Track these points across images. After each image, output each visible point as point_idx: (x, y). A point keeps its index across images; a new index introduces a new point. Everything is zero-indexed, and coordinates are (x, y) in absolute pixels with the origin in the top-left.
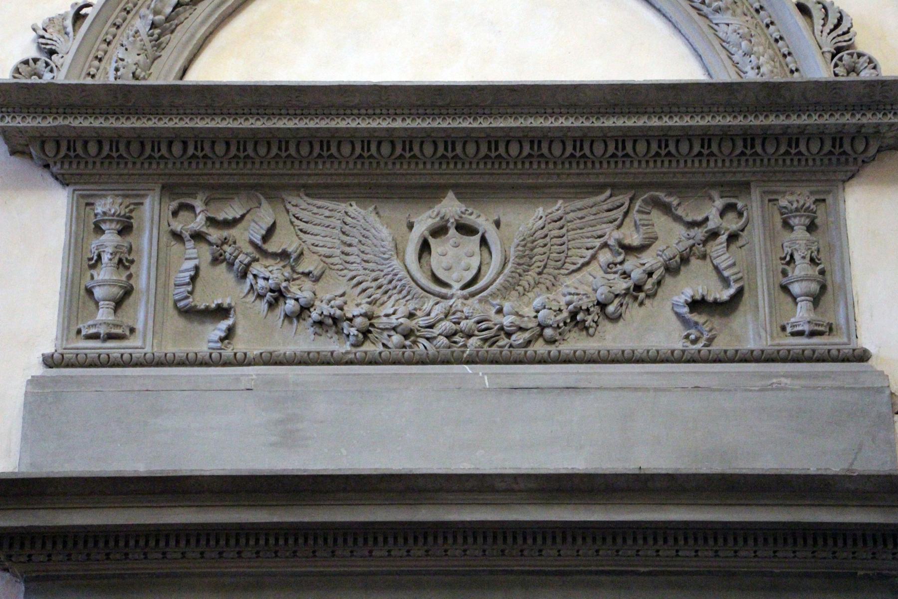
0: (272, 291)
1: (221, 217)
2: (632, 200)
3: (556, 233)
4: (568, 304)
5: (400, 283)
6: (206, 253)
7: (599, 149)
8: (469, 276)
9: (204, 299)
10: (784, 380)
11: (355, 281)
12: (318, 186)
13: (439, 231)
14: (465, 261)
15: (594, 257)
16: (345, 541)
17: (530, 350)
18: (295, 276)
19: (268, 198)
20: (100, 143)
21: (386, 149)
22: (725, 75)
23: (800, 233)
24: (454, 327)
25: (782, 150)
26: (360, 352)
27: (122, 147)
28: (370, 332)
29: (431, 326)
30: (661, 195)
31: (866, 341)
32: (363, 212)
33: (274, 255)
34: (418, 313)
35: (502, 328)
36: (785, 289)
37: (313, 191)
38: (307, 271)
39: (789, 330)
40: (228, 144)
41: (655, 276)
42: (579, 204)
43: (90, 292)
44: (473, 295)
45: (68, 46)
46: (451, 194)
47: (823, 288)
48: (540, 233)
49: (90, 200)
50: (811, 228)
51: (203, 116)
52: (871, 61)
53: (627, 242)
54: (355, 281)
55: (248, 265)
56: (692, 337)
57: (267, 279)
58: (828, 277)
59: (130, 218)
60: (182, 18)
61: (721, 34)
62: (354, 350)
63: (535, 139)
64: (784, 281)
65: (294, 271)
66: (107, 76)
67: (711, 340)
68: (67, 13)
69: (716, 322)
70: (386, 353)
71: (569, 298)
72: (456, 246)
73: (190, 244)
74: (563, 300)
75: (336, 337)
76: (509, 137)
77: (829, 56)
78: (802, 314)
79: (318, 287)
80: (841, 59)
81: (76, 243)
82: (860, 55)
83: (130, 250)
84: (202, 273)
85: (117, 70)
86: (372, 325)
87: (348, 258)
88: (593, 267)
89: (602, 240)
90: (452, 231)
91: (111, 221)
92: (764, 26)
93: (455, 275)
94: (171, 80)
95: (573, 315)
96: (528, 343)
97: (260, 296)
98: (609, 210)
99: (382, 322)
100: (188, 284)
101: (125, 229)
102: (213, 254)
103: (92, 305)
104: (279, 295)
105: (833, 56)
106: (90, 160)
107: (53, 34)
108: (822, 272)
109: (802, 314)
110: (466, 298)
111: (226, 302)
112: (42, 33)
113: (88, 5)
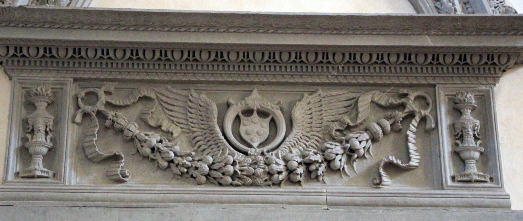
27: (330, 56)
106: (32, 61)
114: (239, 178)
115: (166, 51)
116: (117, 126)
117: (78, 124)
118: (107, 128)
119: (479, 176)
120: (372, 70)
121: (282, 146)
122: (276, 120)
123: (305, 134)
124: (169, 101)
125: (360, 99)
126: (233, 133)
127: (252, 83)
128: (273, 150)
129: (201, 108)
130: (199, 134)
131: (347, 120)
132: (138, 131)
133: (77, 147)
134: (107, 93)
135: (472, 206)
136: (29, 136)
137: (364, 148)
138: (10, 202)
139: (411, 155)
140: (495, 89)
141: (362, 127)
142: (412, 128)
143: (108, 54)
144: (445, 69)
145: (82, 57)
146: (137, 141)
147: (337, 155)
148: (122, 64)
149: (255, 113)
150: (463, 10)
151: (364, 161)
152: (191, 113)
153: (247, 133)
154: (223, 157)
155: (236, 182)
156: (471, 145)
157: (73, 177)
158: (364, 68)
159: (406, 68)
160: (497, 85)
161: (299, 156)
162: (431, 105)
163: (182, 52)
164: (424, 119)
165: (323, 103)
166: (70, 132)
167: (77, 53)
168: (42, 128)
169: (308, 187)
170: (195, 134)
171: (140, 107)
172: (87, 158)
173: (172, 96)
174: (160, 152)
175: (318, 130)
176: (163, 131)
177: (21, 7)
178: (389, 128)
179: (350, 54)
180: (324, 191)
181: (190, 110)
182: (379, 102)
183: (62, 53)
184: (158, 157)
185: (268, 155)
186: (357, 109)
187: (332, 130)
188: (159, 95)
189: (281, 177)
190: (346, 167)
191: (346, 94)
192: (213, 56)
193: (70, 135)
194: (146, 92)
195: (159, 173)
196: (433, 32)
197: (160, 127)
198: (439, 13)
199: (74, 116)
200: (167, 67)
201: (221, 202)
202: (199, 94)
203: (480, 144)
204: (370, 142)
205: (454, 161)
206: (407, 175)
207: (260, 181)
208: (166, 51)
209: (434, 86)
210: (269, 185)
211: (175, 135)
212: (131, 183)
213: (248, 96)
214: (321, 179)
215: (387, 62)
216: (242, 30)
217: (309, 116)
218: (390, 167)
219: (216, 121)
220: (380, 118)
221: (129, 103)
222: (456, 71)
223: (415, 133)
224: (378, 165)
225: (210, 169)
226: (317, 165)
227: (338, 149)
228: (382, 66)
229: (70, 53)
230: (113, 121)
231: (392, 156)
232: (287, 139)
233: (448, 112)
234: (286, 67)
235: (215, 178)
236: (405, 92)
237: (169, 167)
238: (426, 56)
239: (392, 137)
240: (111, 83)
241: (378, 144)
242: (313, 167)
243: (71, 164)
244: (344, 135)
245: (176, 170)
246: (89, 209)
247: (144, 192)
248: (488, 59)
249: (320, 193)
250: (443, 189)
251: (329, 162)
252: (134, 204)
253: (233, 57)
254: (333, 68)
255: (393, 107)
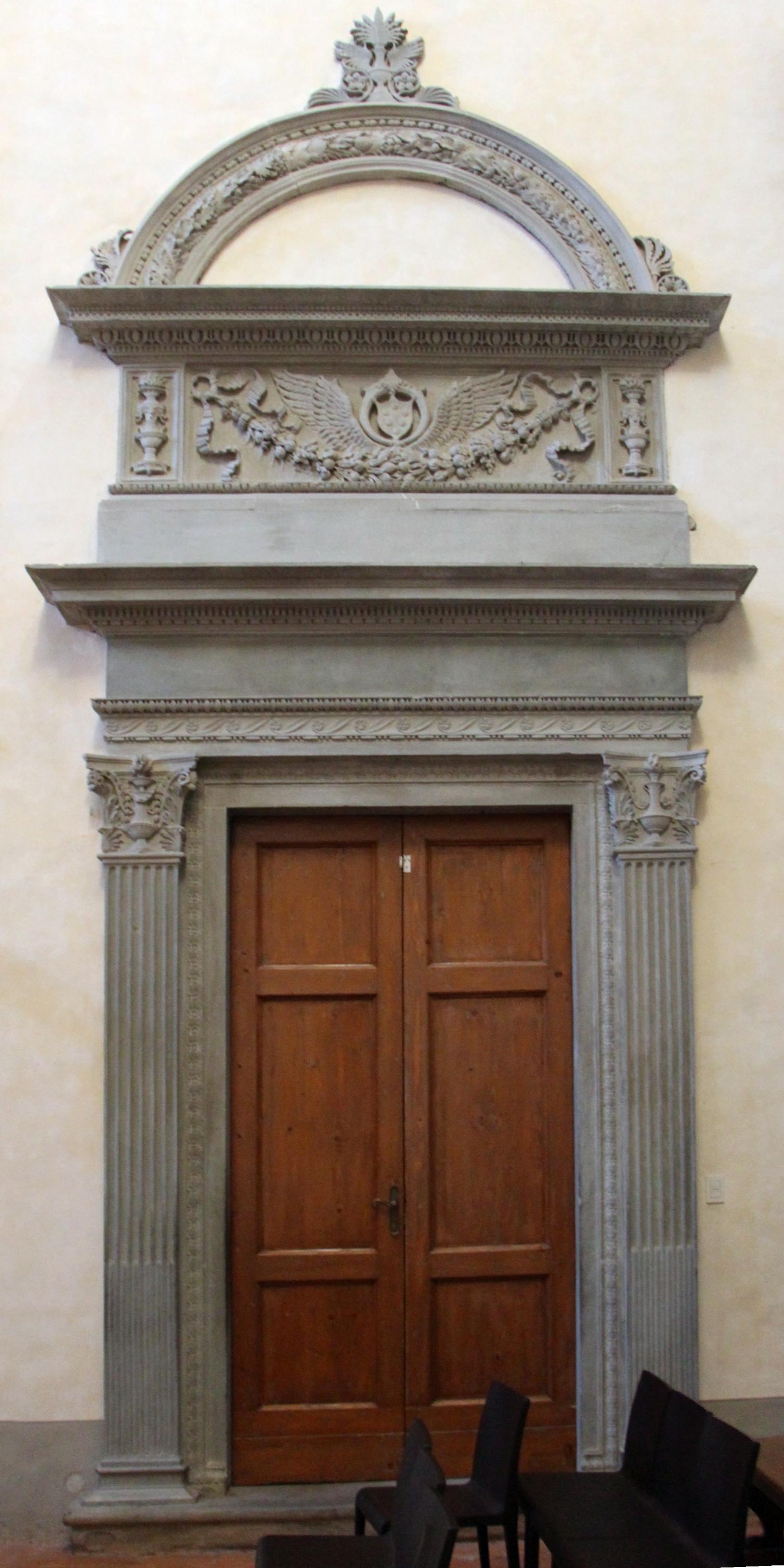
0: (265, 440)
1: (228, 386)
2: (520, 378)
3: (466, 400)
4: (474, 451)
5: (355, 435)
6: (217, 413)
7: (496, 338)
8: (404, 430)
9: (217, 446)
10: (620, 506)
11: (324, 434)
12: (296, 364)
13: (383, 398)
14: (403, 419)
15: (492, 418)
16: (321, 613)
17: (448, 484)
18: (282, 430)
19: (261, 373)
20: (141, 333)
21: (345, 337)
22: (584, 287)
23: (634, 404)
24: (395, 466)
25: (623, 344)
26: (328, 484)
28: (335, 470)
29: (378, 466)
30: (540, 375)
31: (674, 480)
32: (329, 383)
33: (266, 415)
34: (369, 456)
35: (428, 468)
36: (622, 443)
37: (294, 368)
38: (289, 426)
39: (624, 472)
40: (231, 333)
41: (535, 433)
42: (482, 379)
43: (138, 441)
44: (407, 444)
45: (117, 263)
46: (391, 372)
47: (648, 443)
48: (455, 400)
49: (136, 375)
50: (641, 401)
51: (213, 311)
52: (683, 283)
53: (516, 407)
54: (324, 434)
55: (248, 422)
56: (559, 476)
57: (261, 431)
58: (651, 436)
59: (164, 388)
60: (196, 240)
61: (582, 259)
62: (323, 482)
63: (451, 331)
64: (622, 438)
65: (280, 425)
66: (145, 282)
67: (571, 479)
68: (115, 239)
69: (576, 465)
70: (346, 484)
71: (475, 447)
72: (396, 408)
73: (207, 406)
74: (471, 449)
75: (311, 473)
76: (432, 329)
77: (655, 278)
78: (633, 461)
79: (298, 438)
80: (663, 281)
81: (127, 407)
82: (676, 279)
83: (165, 411)
84: (216, 427)
85: (151, 279)
86: (337, 465)
87: (318, 417)
88: (492, 426)
89: (498, 406)
90: (393, 398)
91: (151, 390)
92: (611, 254)
93: (395, 430)
94: (191, 284)
95: (478, 459)
96: (446, 478)
97: (257, 444)
98: (504, 385)
99: (343, 463)
100: (205, 435)
101: (161, 396)
102: (223, 414)
103: (140, 450)
104: (270, 443)
105: (659, 278)
107: (105, 254)
108: (648, 432)
109: (633, 461)
110: (402, 446)
111: (233, 447)
112: (98, 253)
113: (129, 232)
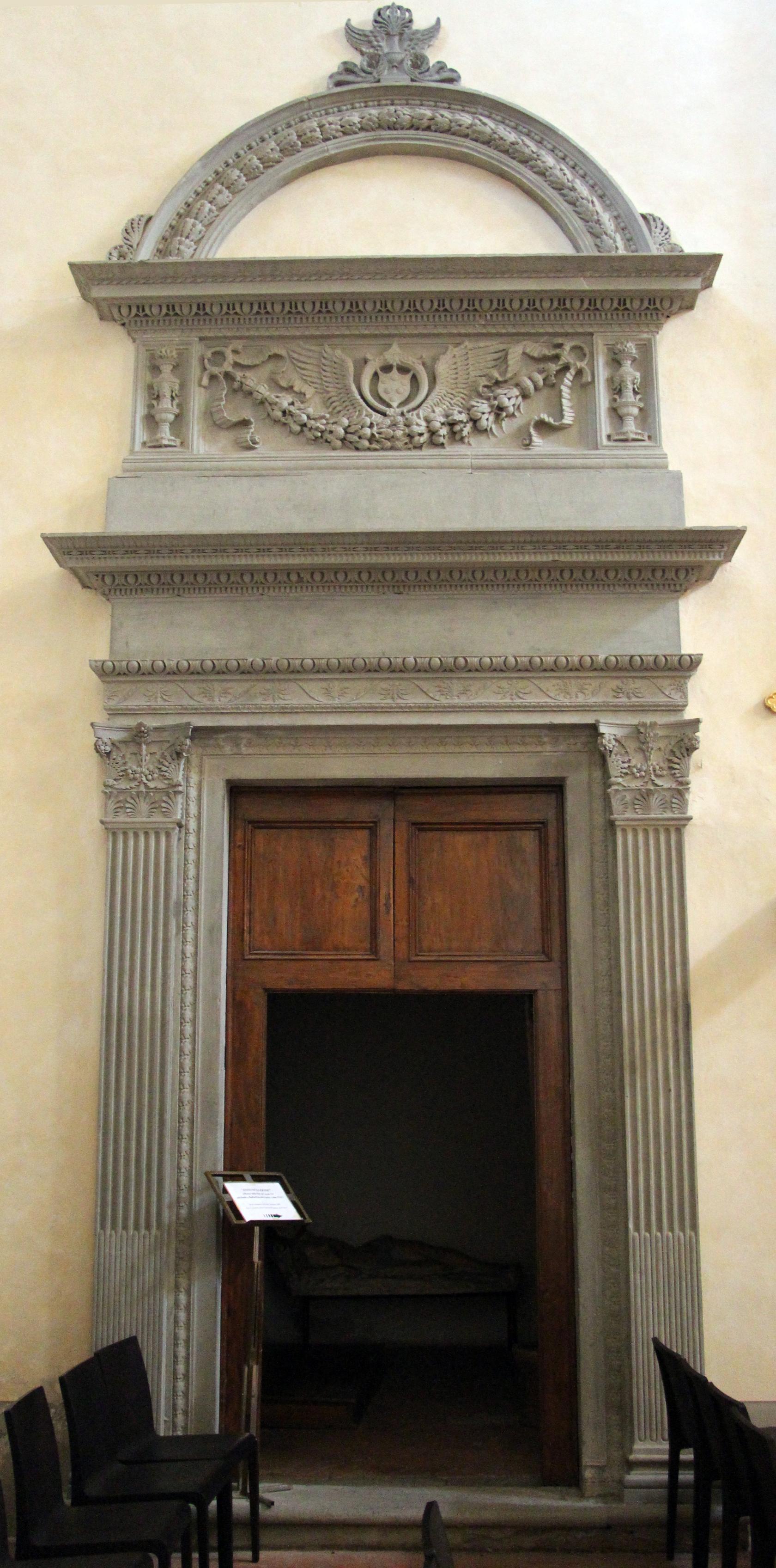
114: (377, 442)
115: (296, 304)
116: (245, 388)
117: (205, 387)
118: (235, 391)
119: (636, 434)
120: (523, 318)
121: (424, 405)
122: (418, 377)
123: (450, 391)
124: (302, 359)
125: (510, 351)
126: (372, 396)
127: (390, 336)
128: (414, 409)
129: (336, 366)
130: (333, 394)
131: (496, 375)
132: (268, 393)
133: (205, 413)
134: (235, 352)
135: (627, 467)
136: (155, 402)
137: (514, 405)
138: (138, 474)
139: (564, 413)
140: (658, 337)
141: (513, 382)
142: (566, 381)
143: (234, 309)
144: (603, 314)
145: (206, 314)
146: (267, 404)
147: (483, 413)
148: (250, 319)
149: (395, 370)
150: (626, 248)
151: (515, 420)
152: (324, 371)
153: (386, 392)
154: (360, 419)
155: (374, 446)
156: (630, 400)
157: (201, 444)
158: (515, 315)
159: (561, 315)
160: (660, 332)
161: (443, 416)
162: (588, 356)
163: (314, 303)
164: (579, 373)
165: (469, 356)
166: (197, 398)
167: (201, 309)
168: (168, 395)
169: (451, 449)
170: (330, 395)
171: (270, 367)
172: (216, 424)
173: (304, 352)
174: (292, 416)
175: (464, 386)
176: (296, 393)
177: (142, 263)
178: (541, 383)
179: (499, 300)
180: (469, 453)
181: (324, 368)
182: (531, 354)
183: (186, 310)
184: (289, 420)
185: (409, 416)
186: (507, 362)
187: (478, 385)
188: (291, 353)
189: (422, 439)
190: (494, 427)
191: (495, 345)
192: (348, 307)
193: (197, 400)
194: (276, 350)
195: (291, 439)
196: (588, 274)
197: (291, 387)
198: (599, 251)
199: (201, 380)
200: (298, 321)
201: (358, 468)
202: (333, 349)
203: (640, 400)
204: (520, 398)
205: (611, 417)
206: (560, 435)
207: (399, 444)
208: (296, 304)
209: (592, 334)
210: (410, 449)
211: (308, 396)
212: (261, 449)
213: (386, 350)
214: (466, 440)
215: (539, 308)
216: (378, 277)
217: (455, 371)
218: (541, 426)
219: (351, 379)
220: (532, 371)
221: (258, 363)
222: (615, 317)
223: (570, 388)
224: (529, 424)
225: (346, 432)
226: (462, 425)
227: (484, 407)
228: (535, 313)
229: (195, 309)
230: (242, 383)
231: (544, 413)
232: (429, 398)
233: (607, 364)
234: (428, 316)
235: (351, 442)
236: (560, 342)
237: (302, 431)
238: (582, 301)
239: (545, 392)
240: (238, 341)
241: (529, 401)
242: (457, 428)
243: (199, 431)
244: (492, 391)
245: (310, 435)
246: (218, 479)
247: (276, 459)
248: (650, 304)
249: (464, 456)
250: (597, 449)
251: (475, 421)
252: (264, 472)
253: (369, 307)
254: (480, 316)
255: (545, 359)
